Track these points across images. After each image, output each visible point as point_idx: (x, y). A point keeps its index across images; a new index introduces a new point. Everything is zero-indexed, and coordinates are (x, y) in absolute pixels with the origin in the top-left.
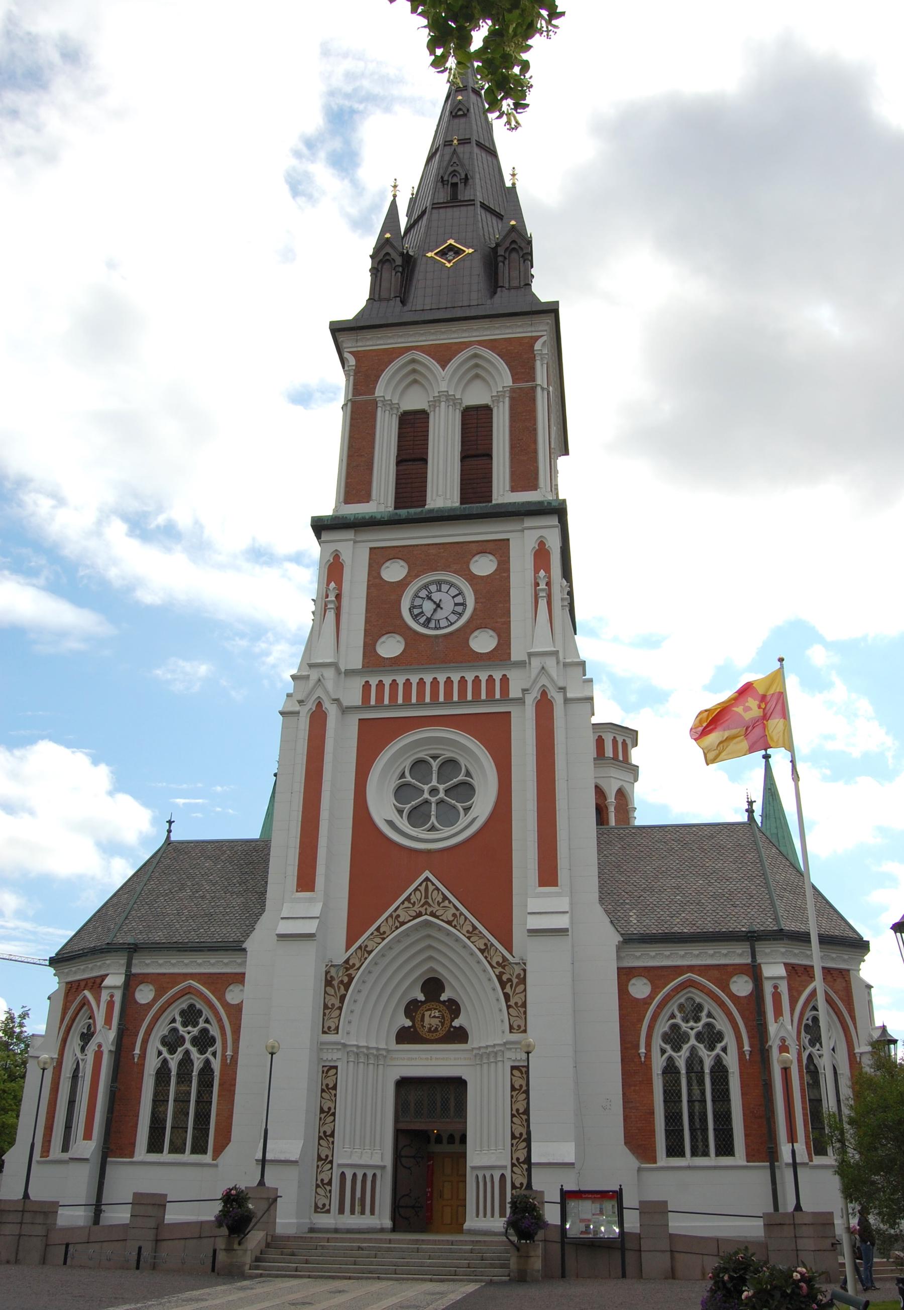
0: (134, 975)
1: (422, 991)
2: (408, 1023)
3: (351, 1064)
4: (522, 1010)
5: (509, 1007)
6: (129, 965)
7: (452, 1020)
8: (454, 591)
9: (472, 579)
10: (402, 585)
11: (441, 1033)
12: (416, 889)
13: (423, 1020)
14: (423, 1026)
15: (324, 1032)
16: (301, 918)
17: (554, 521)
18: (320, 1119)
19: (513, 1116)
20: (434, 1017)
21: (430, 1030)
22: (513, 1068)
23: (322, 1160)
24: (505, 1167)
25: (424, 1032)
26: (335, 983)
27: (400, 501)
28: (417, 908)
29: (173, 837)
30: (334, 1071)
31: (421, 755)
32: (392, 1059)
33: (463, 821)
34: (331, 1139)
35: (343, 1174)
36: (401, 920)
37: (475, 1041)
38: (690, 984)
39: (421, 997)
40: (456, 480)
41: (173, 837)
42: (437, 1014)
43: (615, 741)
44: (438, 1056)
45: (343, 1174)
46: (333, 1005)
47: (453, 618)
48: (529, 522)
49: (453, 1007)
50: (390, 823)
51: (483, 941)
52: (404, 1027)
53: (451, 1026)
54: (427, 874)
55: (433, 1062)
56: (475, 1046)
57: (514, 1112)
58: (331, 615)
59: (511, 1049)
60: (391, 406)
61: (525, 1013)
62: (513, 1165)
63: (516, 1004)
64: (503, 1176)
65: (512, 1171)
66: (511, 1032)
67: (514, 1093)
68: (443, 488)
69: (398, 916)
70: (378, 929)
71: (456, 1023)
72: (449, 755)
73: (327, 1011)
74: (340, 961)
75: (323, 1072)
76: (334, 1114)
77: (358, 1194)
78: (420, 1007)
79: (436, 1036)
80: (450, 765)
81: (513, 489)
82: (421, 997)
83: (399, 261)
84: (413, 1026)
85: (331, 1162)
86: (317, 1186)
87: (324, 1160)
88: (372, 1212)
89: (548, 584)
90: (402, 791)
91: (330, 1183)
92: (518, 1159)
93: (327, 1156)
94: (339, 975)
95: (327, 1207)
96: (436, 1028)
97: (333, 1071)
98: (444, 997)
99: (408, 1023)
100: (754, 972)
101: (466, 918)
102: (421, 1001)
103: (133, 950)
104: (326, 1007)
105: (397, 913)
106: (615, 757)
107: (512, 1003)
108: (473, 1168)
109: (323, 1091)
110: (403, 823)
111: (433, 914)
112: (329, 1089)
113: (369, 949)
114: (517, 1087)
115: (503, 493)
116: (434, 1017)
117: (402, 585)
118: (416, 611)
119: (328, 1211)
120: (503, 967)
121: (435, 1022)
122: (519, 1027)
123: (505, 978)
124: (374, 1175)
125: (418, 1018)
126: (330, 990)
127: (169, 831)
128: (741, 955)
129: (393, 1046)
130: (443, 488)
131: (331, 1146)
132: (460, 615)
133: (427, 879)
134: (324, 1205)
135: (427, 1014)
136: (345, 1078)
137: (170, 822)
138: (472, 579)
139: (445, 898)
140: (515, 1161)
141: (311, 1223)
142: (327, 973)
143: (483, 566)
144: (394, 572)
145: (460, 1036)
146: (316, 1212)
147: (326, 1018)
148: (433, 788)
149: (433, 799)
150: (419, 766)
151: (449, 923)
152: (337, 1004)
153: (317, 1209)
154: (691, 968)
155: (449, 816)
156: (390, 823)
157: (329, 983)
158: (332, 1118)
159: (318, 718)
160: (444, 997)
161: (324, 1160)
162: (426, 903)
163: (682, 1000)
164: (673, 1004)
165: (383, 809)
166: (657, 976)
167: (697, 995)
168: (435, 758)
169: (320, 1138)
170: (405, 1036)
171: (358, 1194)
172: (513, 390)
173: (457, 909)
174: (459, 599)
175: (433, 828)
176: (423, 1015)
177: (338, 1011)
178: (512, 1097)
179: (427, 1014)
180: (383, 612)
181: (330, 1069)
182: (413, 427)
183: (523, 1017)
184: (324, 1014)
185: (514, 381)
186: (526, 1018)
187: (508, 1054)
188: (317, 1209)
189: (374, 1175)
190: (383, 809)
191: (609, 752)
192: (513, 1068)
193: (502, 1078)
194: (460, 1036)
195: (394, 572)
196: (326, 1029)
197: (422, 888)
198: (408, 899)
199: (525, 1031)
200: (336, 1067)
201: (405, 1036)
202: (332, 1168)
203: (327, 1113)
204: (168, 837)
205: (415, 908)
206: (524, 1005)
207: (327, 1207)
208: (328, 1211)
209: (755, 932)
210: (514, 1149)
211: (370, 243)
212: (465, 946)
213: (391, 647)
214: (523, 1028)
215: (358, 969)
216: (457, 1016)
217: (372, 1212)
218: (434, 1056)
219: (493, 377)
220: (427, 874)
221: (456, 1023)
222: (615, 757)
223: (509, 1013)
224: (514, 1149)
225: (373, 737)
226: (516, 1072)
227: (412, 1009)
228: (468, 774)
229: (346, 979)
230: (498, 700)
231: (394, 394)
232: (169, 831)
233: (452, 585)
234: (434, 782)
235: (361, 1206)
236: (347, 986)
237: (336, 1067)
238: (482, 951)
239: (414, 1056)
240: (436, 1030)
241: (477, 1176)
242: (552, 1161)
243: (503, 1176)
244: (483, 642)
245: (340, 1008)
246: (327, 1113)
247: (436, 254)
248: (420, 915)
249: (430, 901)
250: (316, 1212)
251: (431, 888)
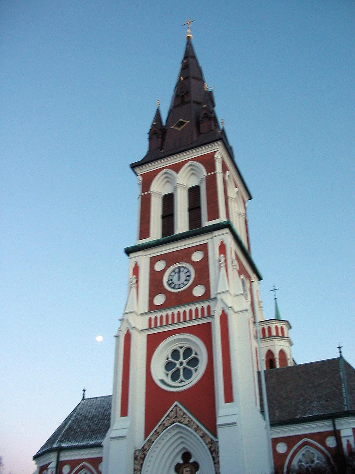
0: (62, 461)
6: (58, 457)
8: (186, 271)
9: (193, 263)
10: (163, 271)
12: (172, 411)
16: (128, 428)
17: (227, 230)
26: (138, 458)
27: (164, 235)
28: (172, 420)
29: (86, 397)
31: (175, 347)
33: (194, 375)
36: (166, 425)
38: (306, 443)
39: (181, 462)
40: (241, 222)
41: (86, 397)
43: (276, 328)
47: (186, 282)
48: (216, 233)
50: (162, 381)
51: (202, 432)
54: (176, 403)
58: (134, 290)
60: (157, 193)
68: (182, 224)
69: (164, 424)
70: (156, 431)
72: (187, 346)
74: (140, 448)
80: (188, 351)
81: (209, 220)
82: (181, 462)
83: (160, 132)
89: (226, 260)
90: (169, 366)
94: (140, 454)
98: (191, 461)
100: (336, 434)
101: (194, 422)
103: (60, 450)
105: (164, 423)
106: (277, 335)
110: (169, 381)
111: (179, 422)
113: (152, 441)
115: (206, 223)
117: (163, 271)
118: (170, 282)
120: (212, 444)
123: (212, 449)
126: (136, 462)
127: (84, 395)
128: (329, 426)
130: (182, 224)
132: (188, 280)
133: (176, 405)
135: (185, 469)
137: (84, 391)
138: (193, 263)
139: (184, 414)
142: (135, 453)
143: (197, 257)
144: (160, 266)
148: (182, 363)
149: (181, 367)
150: (175, 354)
151: (186, 425)
154: (306, 436)
155: (188, 374)
156: (162, 381)
157: (136, 458)
159: (128, 337)
160: (191, 461)
162: (176, 417)
163: (304, 452)
165: (159, 373)
166: (290, 441)
167: (311, 449)
168: (181, 348)
172: (207, 177)
173: (190, 418)
174: (188, 274)
175: (182, 381)
176: (183, 471)
180: (156, 284)
182: (169, 201)
185: (208, 173)
190: (159, 373)
191: (274, 333)
195: (160, 266)
197: (174, 410)
198: (168, 416)
204: (83, 397)
205: (171, 420)
209: (333, 414)
211: (148, 127)
212: (195, 436)
213: (159, 300)
215: (148, 450)
219: (197, 171)
220: (176, 403)
222: (277, 335)
225: (153, 342)
228: (196, 354)
229: (143, 456)
230: (200, 318)
231: (159, 188)
232: (84, 395)
233: (185, 268)
234: (181, 359)
236: (143, 459)
238: (202, 437)
244: (199, 291)
247: (175, 126)
248: (173, 423)
249: (178, 415)
251: (178, 409)
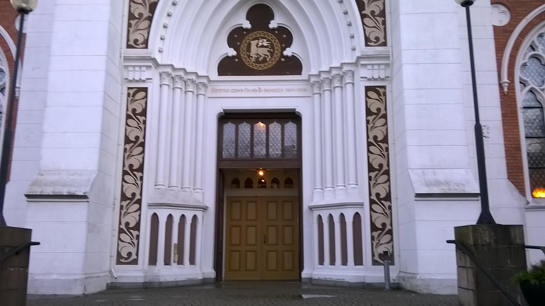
1: (248, 18)
2: (232, 52)
3: (165, 88)
4: (380, 20)
5: (363, 16)
7: (284, 49)
11: (271, 63)
13: (249, 49)
14: (249, 56)
15: (129, 46)
18: (125, 150)
19: (369, 144)
20: (263, 46)
21: (257, 61)
22: (368, 89)
23: (128, 199)
24: (361, 205)
25: (250, 63)
30: (142, 94)
32: (214, 91)
34: (139, 175)
35: (155, 217)
37: (311, 68)
39: (247, 25)
42: (265, 44)
44: (267, 87)
45: (155, 217)
46: (141, 15)
49: (285, 36)
52: (228, 57)
53: (282, 56)
55: (263, 94)
56: (314, 71)
57: (371, 140)
59: (366, 65)
61: (384, 23)
62: (372, 202)
63: (373, 12)
64: (357, 216)
65: (371, 210)
66: (367, 45)
67: (371, 118)
71: (288, 52)
73: (133, 22)
75: (129, 95)
76: (143, 145)
77: (175, 240)
78: (246, 35)
79: (263, 67)
82: (247, 25)
84: (238, 56)
85: (139, 202)
86: (121, 231)
87: (131, 200)
88: (192, 261)
91: (137, 227)
92: (378, 195)
93: (134, 195)
95: (134, 257)
96: (265, 58)
97: (141, 94)
98: (273, 24)
99: (232, 52)
102: (246, 30)
104: (131, 16)
107: (367, 11)
108: (311, 208)
109: (128, 117)
112: (137, 115)
114: (374, 110)
116: (263, 46)
119: (135, 262)
121: (263, 52)
122: (377, 39)
124: (195, 217)
125: (244, 46)
129: (214, 75)
131: (139, 182)
134: (130, 254)
135: (254, 43)
136: (160, 101)
140: (374, 197)
141: (203, 274)
145: (293, 66)
146: (119, 263)
147: (131, 30)
152: (146, 14)
153: (120, 260)
158: (140, 149)
160: (273, 24)
161: (131, 200)
164: (535, 33)
169: (125, 173)
170: (227, 67)
171: (175, 240)
176: (249, 45)
177: (147, 23)
178: (368, 122)
179: (254, 43)
181: (138, 92)
183: (382, 27)
184: (130, 25)
186: (385, 29)
187: (363, 72)
188: (120, 260)
189: (195, 217)
192: (368, 89)
193: (352, 102)
194: (293, 66)
196: (131, 43)
199: (384, 44)
200: (145, 90)
201: (227, 67)
202: (140, 209)
203: (135, 143)
206: (383, 14)
207: (134, 257)
208: (135, 262)
210: (372, 183)
214: (382, 40)
216: (289, 45)
217: (192, 261)
218: (263, 88)
221: (288, 52)
223: (364, 24)
224: (372, 183)
226: (372, 94)
227: (236, 37)
235: (177, 254)
237: (145, 90)
239: (238, 88)
240: (265, 60)
241: (320, 217)
242: (448, 192)
243: (357, 216)
245: (150, 19)
246: (135, 143)
250: (119, 263)
